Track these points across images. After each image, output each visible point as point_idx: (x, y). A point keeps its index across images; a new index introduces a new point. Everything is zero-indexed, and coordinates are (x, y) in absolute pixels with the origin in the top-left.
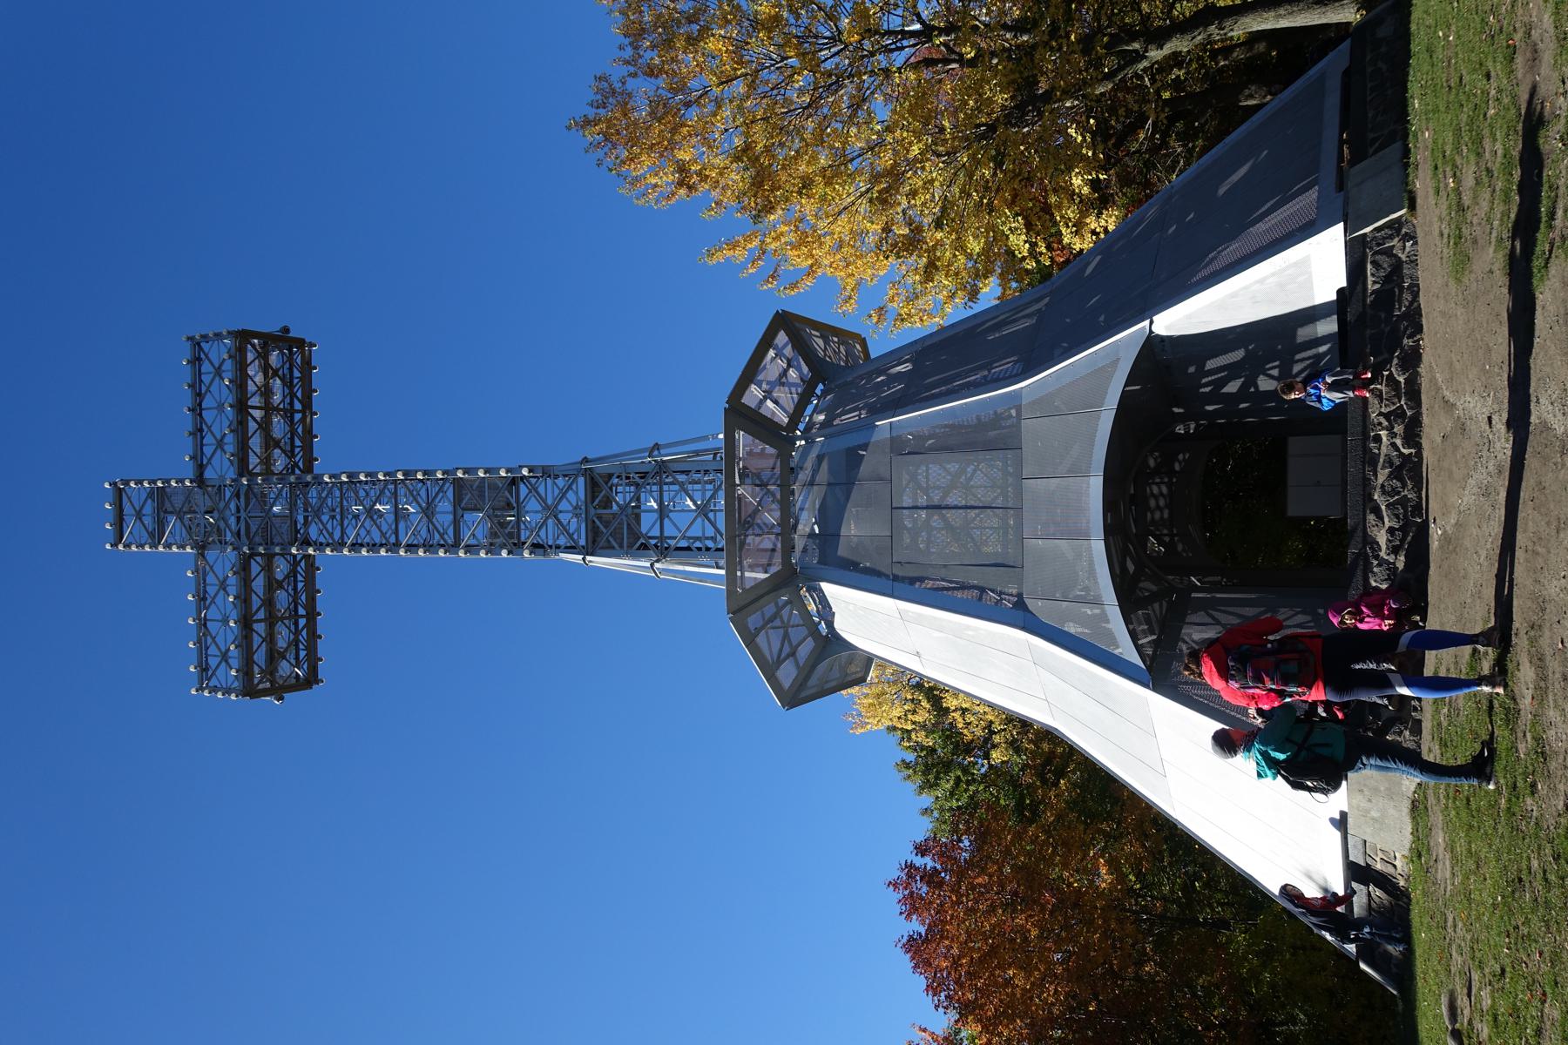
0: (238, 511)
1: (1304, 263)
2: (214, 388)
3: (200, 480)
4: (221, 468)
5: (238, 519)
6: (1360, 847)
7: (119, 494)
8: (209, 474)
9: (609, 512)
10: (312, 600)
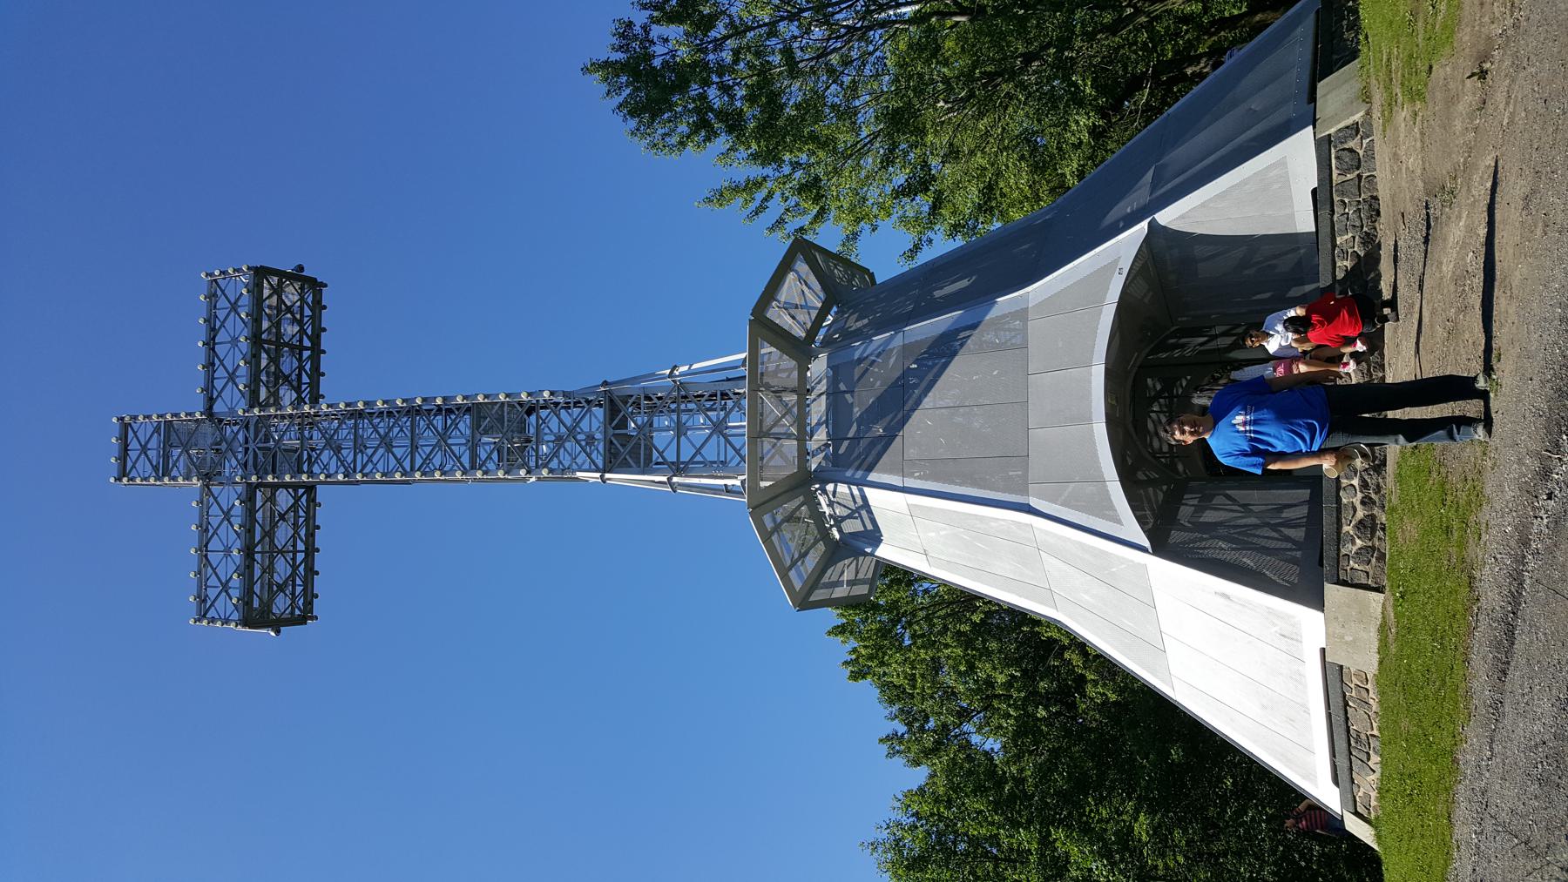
0: (247, 442)
1: (1282, 163)
2: (229, 324)
3: (209, 412)
4: (233, 401)
5: (247, 450)
7: (125, 427)
8: (218, 407)
9: (625, 426)
10: (311, 535)
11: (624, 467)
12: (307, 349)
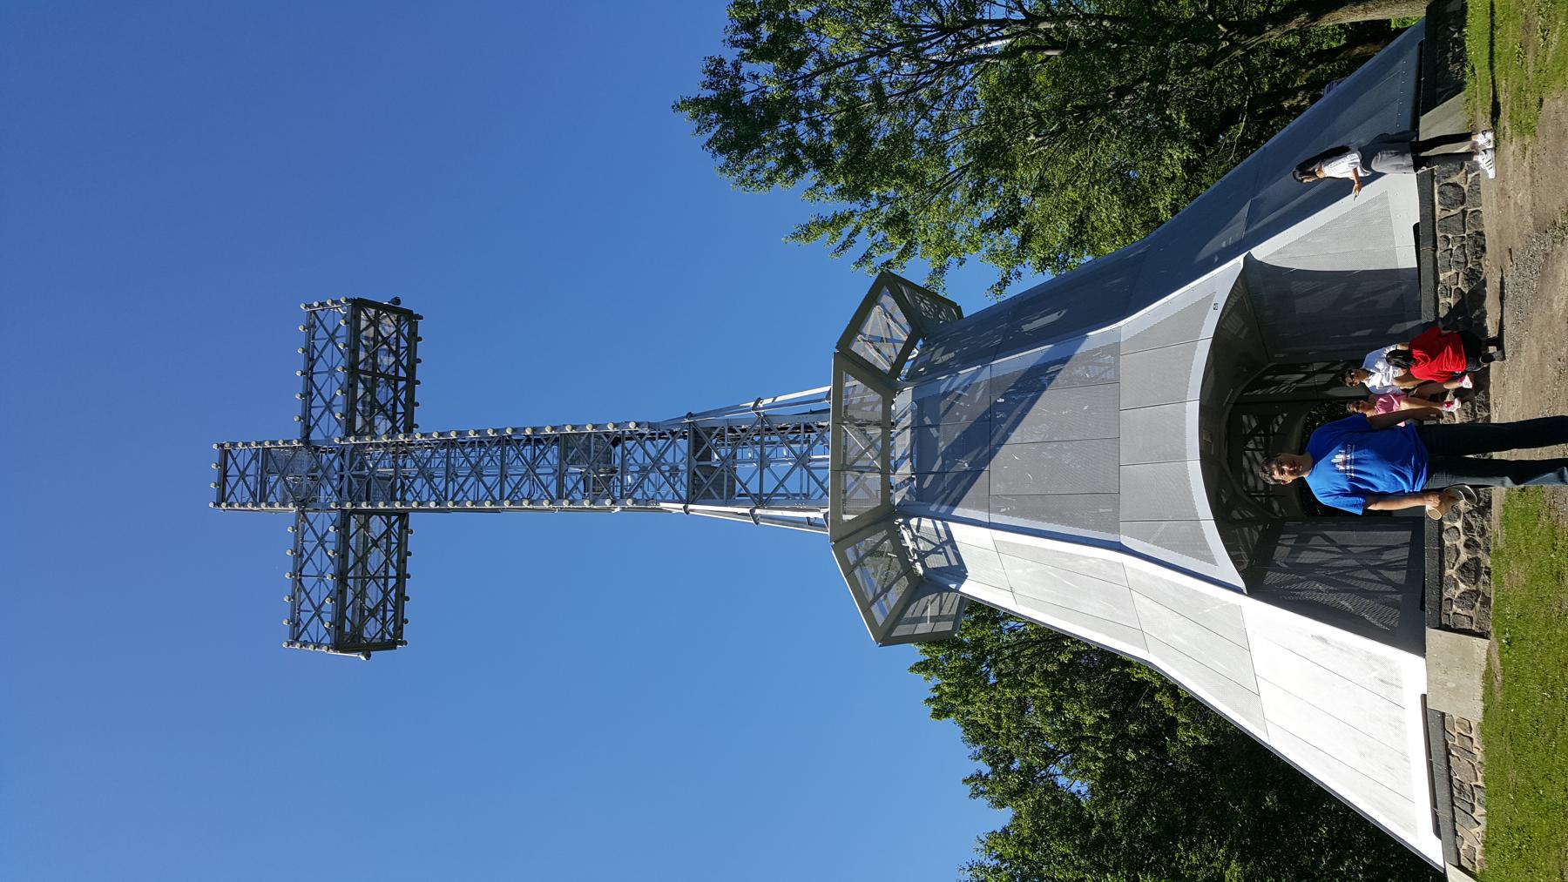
1: (1383, 198)
2: (326, 354)
3: (306, 440)
4: (329, 430)
5: (342, 477)
6: (1439, 722)
7: (225, 454)
9: (708, 458)
11: (707, 498)
12: (402, 379)
